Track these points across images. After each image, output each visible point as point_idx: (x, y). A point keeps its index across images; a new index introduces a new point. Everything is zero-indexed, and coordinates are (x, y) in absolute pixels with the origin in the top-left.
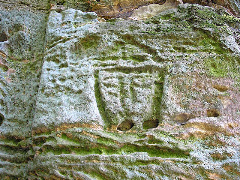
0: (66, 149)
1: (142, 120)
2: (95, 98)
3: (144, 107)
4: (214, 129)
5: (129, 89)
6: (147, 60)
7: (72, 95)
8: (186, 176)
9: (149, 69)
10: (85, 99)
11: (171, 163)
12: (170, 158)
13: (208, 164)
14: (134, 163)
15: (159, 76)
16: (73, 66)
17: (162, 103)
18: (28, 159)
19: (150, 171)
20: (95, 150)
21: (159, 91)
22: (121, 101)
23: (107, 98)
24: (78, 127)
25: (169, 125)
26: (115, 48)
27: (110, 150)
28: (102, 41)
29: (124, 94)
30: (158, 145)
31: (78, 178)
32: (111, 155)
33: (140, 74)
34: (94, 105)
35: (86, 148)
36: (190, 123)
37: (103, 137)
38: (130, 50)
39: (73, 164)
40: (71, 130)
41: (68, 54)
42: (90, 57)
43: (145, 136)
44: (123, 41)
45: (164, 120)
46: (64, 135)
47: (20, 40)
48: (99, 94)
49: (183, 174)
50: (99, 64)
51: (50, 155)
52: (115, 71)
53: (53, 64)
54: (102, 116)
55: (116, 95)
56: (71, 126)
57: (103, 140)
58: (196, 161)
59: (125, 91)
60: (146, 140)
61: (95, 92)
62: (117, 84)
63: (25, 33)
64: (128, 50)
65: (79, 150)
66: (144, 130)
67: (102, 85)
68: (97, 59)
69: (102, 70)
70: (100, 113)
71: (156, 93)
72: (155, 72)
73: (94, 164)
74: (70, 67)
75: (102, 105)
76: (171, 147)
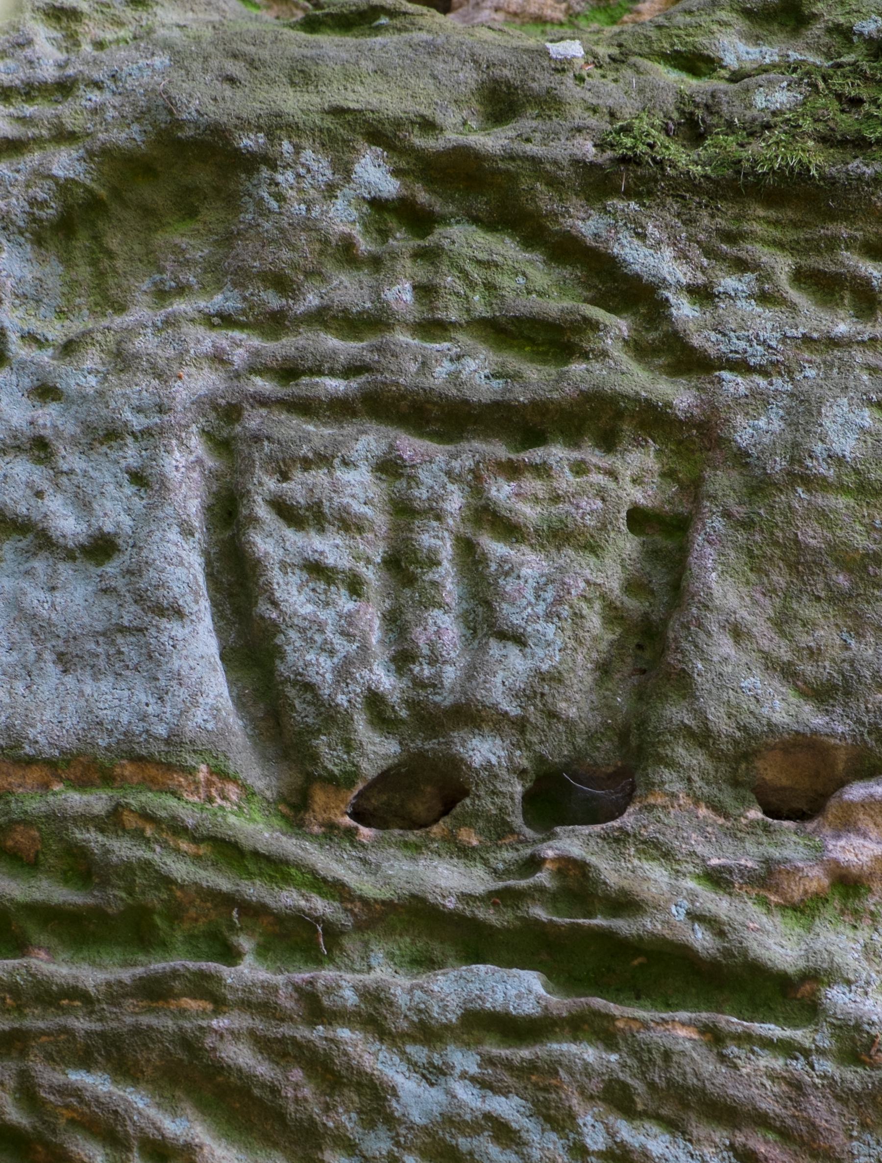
1: (525, 763)
2: (205, 604)
3: (542, 677)
5: (446, 550)
6: (585, 356)
7: (39, 565)
8: (785, 1134)
10: (140, 598)
11: (688, 1045)
12: (684, 1015)
14: (447, 1027)
15: (668, 474)
16: (45, 357)
17: (672, 658)
19: (553, 1082)
20: (191, 939)
21: (659, 579)
22: (489, 690)
24: (82, 784)
25: (703, 811)
26: (365, 245)
28: (273, 189)
29: (409, 580)
30: (623, 926)
31: (75, 1110)
32: (302, 976)
33: (535, 455)
36: (851, 805)
37: (256, 854)
38: (476, 274)
39: (41, 1024)
40: (34, 805)
42: (180, 306)
43: (534, 864)
44: (423, 197)
45: (667, 774)
49: (762, 1120)
50: (239, 357)
52: (354, 414)
54: (252, 721)
55: (355, 586)
56: (35, 774)
57: (250, 875)
59: (418, 562)
60: (540, 889)
61: (206, 553)
62: (364, 509)
64: (462, 271)
66: (529, 833)
67: (262, 511)
68: (226, 320)
69: (262, 401)
70: (240, 702)
71: (632, 587)
72: (639, 444)
73: (187, 1025)
74: (23, 365)
76: (697, 946)
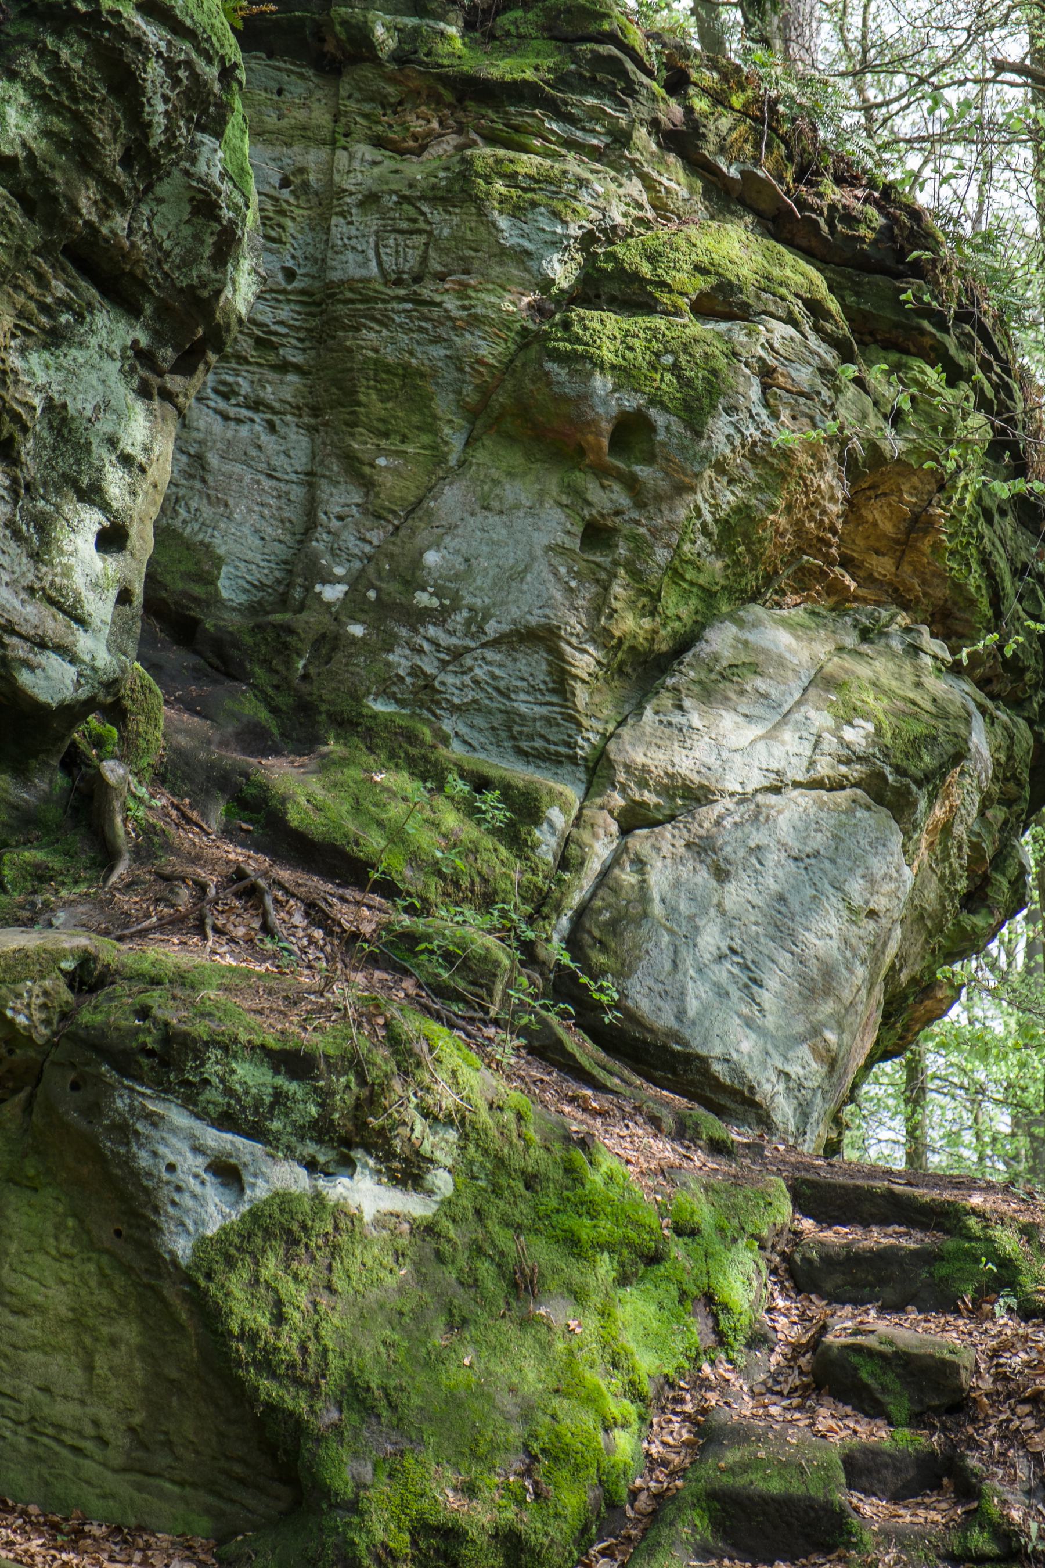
0: (352, 301)
4: (466, 286)
9: (419, 232)
13: (455, 313)
18: (322, 313)
23: (384, 257)
27: (384, 301)
34: (373, 264)
35: (366, 300)
41: (354, 211)
46: (352, 290)
47: (306, 184)
48: (378, 255)
51: (340, 306)
53: (341, 220)
58: (446, 311)
63: (312, 178)
65: (361, 301)
75: (380, 264)
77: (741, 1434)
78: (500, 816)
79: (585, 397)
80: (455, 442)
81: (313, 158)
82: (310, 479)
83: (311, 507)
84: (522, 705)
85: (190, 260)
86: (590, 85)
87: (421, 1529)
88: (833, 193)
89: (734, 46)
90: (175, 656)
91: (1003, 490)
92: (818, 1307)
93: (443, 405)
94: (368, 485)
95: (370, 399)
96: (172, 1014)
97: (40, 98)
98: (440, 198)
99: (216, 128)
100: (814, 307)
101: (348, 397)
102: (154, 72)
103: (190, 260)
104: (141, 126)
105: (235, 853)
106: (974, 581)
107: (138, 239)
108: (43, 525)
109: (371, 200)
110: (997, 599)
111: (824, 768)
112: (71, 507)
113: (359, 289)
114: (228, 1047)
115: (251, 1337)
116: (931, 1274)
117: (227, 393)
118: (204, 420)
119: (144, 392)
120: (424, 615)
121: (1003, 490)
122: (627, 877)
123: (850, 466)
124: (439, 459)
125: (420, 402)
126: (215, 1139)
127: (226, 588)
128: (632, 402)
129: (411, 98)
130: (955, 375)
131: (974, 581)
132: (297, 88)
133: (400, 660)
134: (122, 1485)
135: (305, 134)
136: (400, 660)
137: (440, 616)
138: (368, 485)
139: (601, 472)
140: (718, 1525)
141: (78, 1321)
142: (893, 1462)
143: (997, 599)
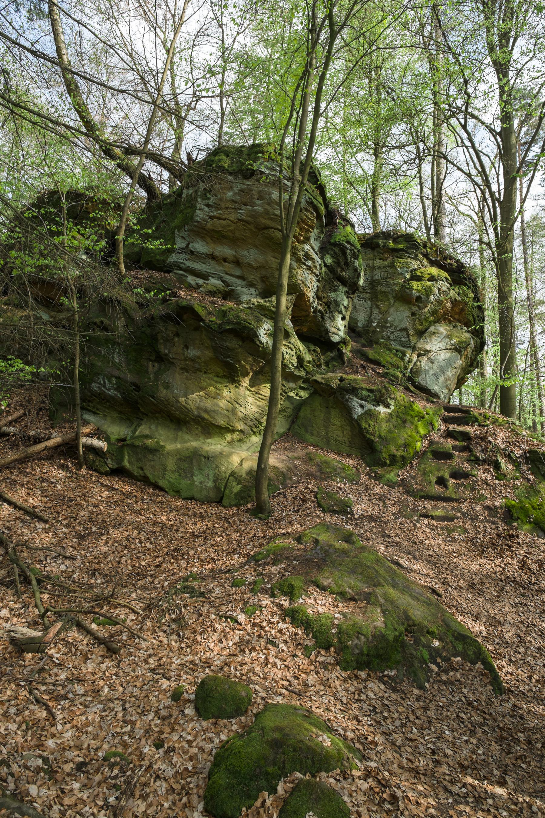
77: (437, 443)
78: (400, 355)
79: (412, 294)
80: (392, 302)
81: (371, 262)
82: (371, 308)
83: (371, 313)
84: (403, 339)
85: (354, 278)
86: (412, 248)
87: (390, 455)
88: (449, 261)
89: (433, 240)
90: (352, 334)
91: (476, 304)
92: (448, 425)
93: (390, 297)
94: (379, 309)
95: (380, 297)
96: (354, 385)
97: (332, 257)
98: (389, 266)
99: (357, 258)
100: (446, 279)
101: (377, 296)
102: (348, 251)
103: (354, 278)
104: (347, 259)
105: (361, 362)
106: (471, 318)
107: (348, 733)
108: (334, 317)
109: (379, 268)
110: (475, 321)
111: (448, 347)
112: (336, 314)
113: (378, 281)
114: (361, 389)
115: (365, 429)
116: (189, 701)
117: (359, 297)
118: (356, 301)
119: (347, 297)
120: (388, 327)
121: (476, 304)
122: (418, 364)
123: (452, 302)
124: (390, 304)
125: (387, 296)
126: (360, 401)
127: (359, 325)
128: (418, 294)
129: (385, 252)
130: (469, 288)
131: (471, 318)
132: (368, 252)
133: (384, 334)
134: (348, 449)
135: (369, 259)
136: (384, 334)
137: (390, 327)
138: (379, 309)
139: (414, 305)
140: (433, 455)
141: (341, 427)
142: (460, 447)
143: (475, 321)
